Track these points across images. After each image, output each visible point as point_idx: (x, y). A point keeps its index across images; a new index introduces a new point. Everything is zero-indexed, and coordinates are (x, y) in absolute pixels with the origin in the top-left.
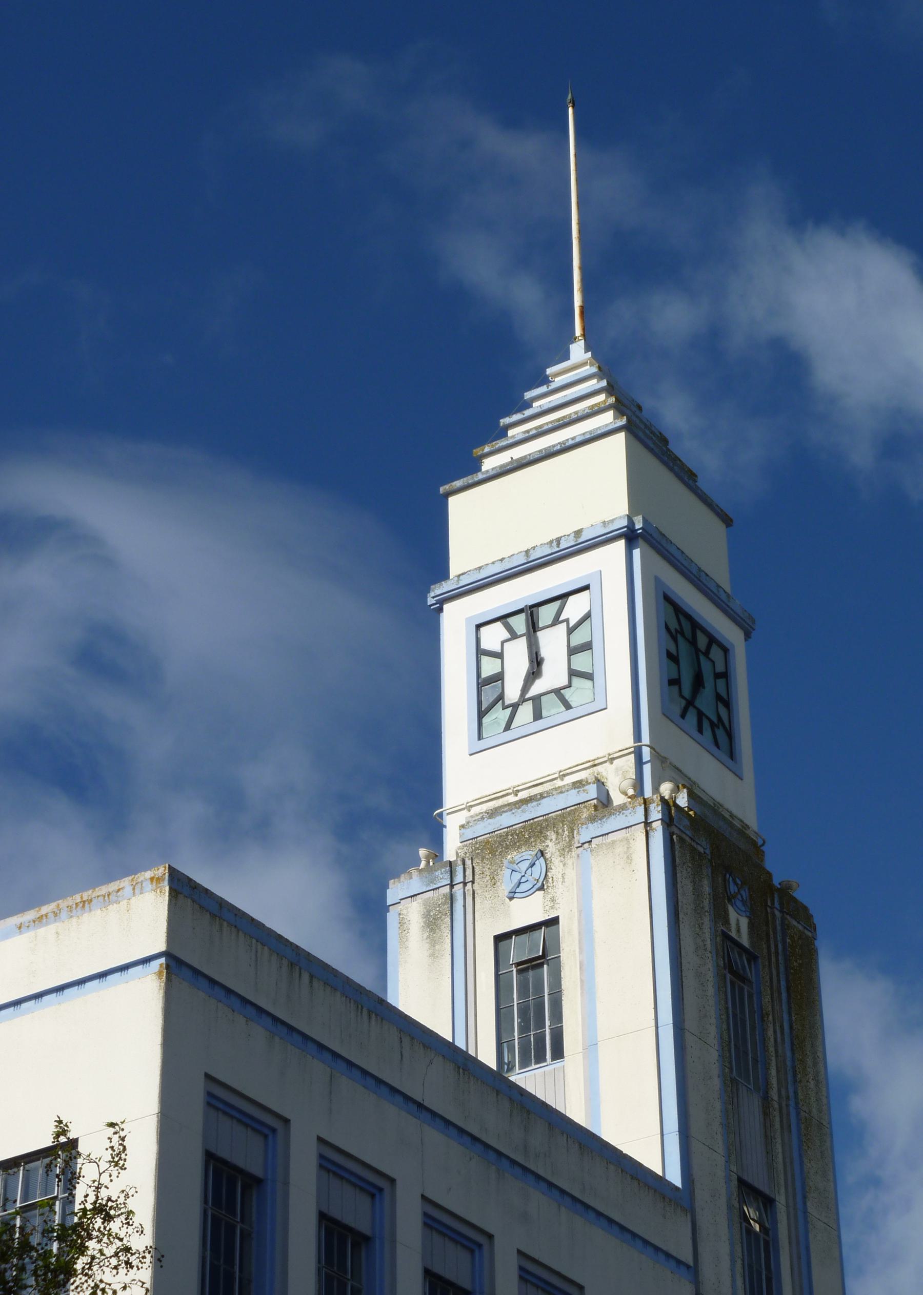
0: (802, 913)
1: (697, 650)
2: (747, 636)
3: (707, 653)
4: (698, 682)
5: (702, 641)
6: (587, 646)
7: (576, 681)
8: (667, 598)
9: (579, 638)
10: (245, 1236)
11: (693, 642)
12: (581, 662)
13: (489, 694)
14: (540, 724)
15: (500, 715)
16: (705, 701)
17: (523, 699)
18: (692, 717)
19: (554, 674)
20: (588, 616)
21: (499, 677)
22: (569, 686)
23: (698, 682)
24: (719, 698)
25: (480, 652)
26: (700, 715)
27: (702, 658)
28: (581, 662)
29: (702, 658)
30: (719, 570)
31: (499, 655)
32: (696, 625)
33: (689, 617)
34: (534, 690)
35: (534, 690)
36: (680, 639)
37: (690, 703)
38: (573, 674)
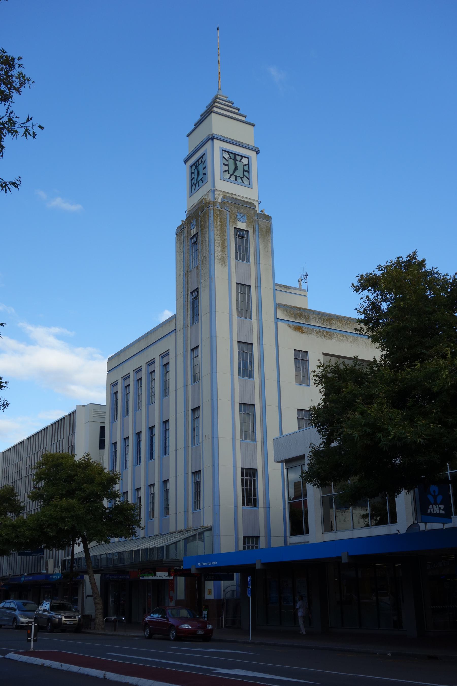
2: (258, 153)
4: (236, 169)
8: (223, 150)
14: (204, 183)
16: (239, 173)
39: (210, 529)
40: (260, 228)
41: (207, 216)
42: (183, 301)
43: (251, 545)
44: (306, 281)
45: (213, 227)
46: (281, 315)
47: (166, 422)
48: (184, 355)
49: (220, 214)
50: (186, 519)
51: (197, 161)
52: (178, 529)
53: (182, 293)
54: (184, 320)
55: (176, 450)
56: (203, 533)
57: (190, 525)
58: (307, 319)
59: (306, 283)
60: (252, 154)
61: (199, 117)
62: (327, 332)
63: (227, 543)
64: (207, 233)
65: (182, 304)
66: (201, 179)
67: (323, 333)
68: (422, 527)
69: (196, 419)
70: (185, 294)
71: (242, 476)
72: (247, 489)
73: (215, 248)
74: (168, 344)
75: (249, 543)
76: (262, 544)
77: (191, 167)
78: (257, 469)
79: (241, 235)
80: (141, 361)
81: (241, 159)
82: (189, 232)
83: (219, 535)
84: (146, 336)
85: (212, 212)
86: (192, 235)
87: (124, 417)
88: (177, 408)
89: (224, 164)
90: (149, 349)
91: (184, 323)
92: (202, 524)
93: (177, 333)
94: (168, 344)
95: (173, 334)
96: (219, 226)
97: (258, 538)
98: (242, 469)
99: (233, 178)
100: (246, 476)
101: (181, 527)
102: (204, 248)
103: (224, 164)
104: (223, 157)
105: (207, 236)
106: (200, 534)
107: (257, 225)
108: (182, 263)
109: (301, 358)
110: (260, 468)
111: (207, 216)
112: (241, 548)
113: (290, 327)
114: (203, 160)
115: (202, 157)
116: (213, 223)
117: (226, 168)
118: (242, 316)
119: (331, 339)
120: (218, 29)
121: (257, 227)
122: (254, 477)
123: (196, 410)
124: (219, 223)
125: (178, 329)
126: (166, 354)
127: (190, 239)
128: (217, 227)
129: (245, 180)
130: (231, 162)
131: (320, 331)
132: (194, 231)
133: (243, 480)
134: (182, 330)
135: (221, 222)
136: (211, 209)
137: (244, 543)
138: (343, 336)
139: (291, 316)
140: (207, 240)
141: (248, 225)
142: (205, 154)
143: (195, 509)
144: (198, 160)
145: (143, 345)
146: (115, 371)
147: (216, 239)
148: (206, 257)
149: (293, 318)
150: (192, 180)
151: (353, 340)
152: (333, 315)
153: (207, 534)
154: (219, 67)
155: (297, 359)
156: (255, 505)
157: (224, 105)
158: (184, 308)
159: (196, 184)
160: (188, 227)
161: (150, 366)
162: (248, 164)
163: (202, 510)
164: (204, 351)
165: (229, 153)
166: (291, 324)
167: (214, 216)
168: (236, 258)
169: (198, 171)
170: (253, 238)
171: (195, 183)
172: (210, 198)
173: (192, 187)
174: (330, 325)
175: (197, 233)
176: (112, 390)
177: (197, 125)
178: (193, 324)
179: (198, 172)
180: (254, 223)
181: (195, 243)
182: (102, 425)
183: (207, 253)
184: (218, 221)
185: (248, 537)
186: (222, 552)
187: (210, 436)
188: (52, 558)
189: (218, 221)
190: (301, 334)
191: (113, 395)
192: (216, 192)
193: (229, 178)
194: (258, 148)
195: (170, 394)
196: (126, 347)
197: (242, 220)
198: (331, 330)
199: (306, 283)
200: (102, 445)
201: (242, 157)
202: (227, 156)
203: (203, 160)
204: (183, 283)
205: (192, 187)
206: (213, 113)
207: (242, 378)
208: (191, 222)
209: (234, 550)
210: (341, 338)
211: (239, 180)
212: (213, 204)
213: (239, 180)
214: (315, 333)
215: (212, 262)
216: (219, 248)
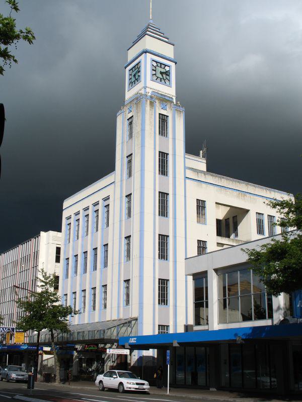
2: (176, 63)
39: (136, 319)
47: (106, 245)
51: (133, 68)
52: (113, 319)
56: (130, 322)
60: (173, 65)
63: (148, 329)
69: (130, 162)
71: (159, 284)
72: (162, 293)
75: (162, 330)
76: (171, 331)
78: (169, 280)
81: (165, 67)
83: (142, 323)
89: (153, 70)
92: (130, 316)
95: (113, 185)
97: (168, 326)
98: (159, 279)
100: (162, 284)
101: (115, 317)
103: (153, 70)
104: (153, 65)
106: (130, 322)
109: (201, 206)
110: (170, 152)
112: (157, 333)
114: (139, 67)
115: (137, 64)
117: (154, 72)
118: (162, 174)
122: (167, 285)
123: (129, 196)
125: (116, 181)
126: (107, 198)
129: (167, 81)
133: (159, 287)
137: (159, 330)
144: (135, 67)
153: (133, 322)
155: (198, 207)
157: (156, 34)
163: (131, 306)
164: (135, 241)
165: (156, 62)
168: (159, 215)
172: (143, 92)
182: (58, 246)
185: (162, 326)
192: (147, 88)
200: (58, 260)
201: (166, 66)
202: (155, 64)
203: (139, 67)
206: (146, 36)
207: (161, 176)
209: (152, 334)
211: (163, 81)
213: (163, 81)
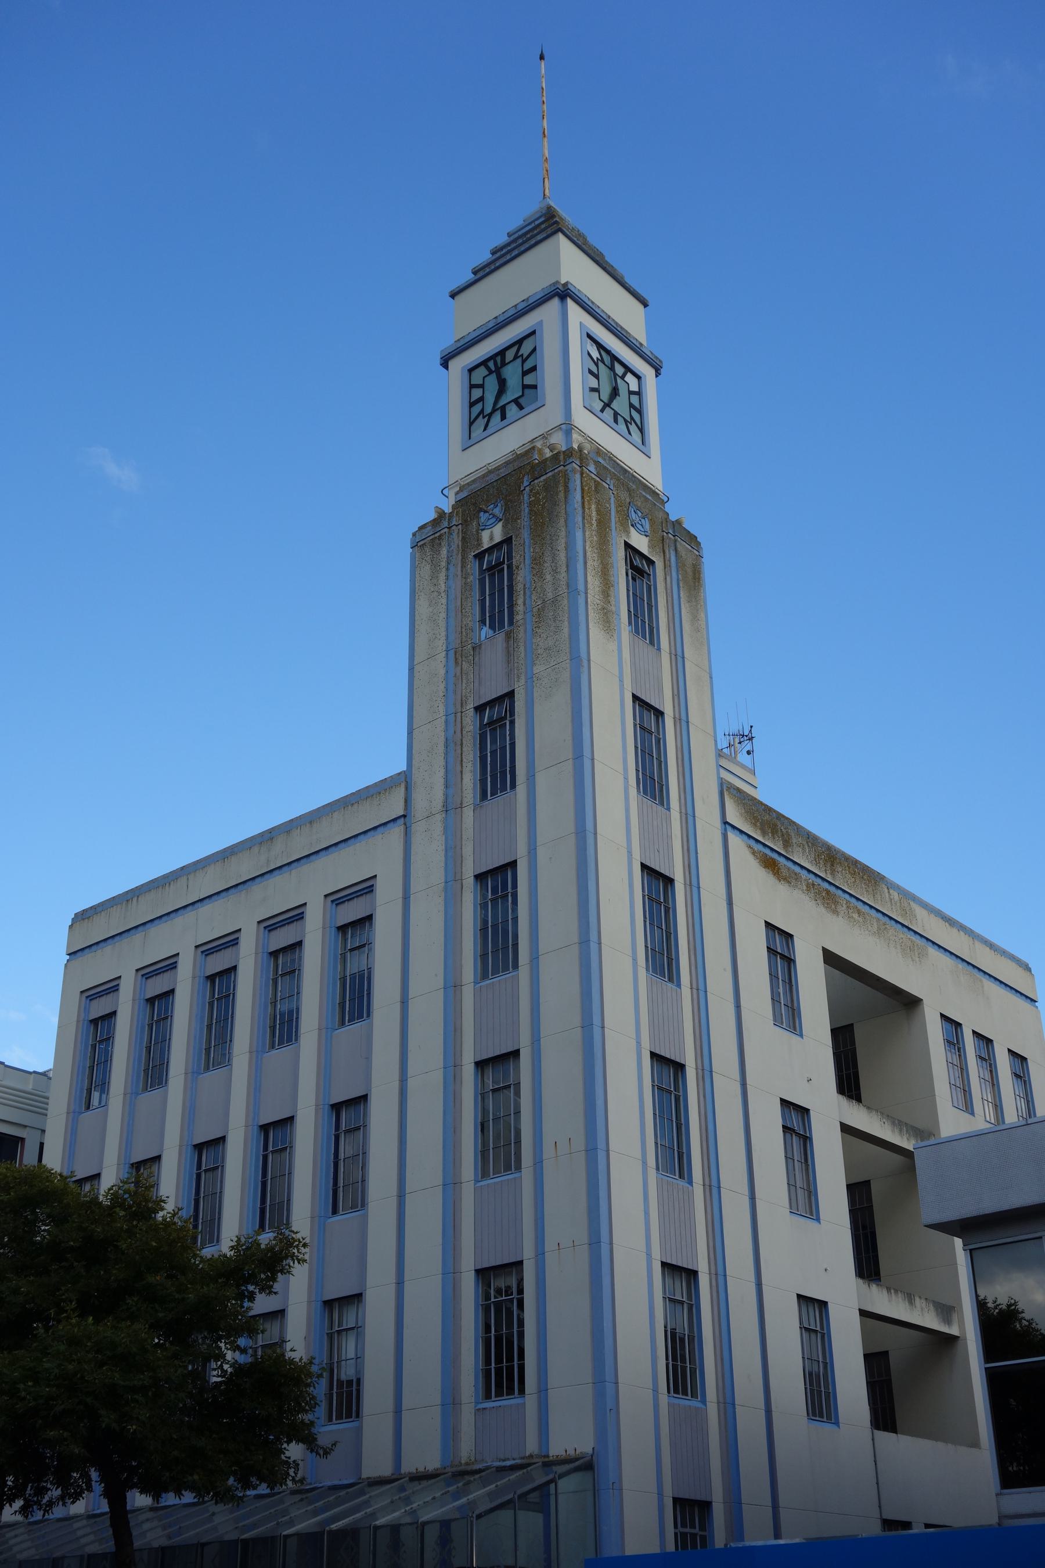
0: (692, 539)
1: (615, 375)
2: (658, 373)
3: (623, 377)
4: (615, 392)
5: (619, 370)
6: (534, 369)
7: (527, 391)
8: (589, 336)
9: (528, 365)
10: (693, 1372)
11: (612, 368)
12: (529, 380)
13: (477, 409)
14: (505, 422)
15: (481, 422)
16: (620, 405)
17: (494, 411)
18: (608, 414)
19: (513, 391)
20: (534, 350)
21: (481, 399)
22: (523, 395)
23: (615, 392)
24: (631, 406)
25: (472, 387)
26: (616, 415)
27: (619, 380)
28: (529, 380)
29: (619, 380)
30: (638, 331)
31: (482, 386)
32: (614, 358)
33: (608, 352)
34: (501, 403)
35: (501, 403)
36: (600, 364)
37: (607, 405)
38: (525, 387)
39: (585, 1465)
40: (681, 565)
41: (561, 488)
42: (446, 730)
43: (688, 1530)
44: (749, 748)
45: (580, 519)
46: (734, 816)
48: (446, 890)
49: (597, 491)
50: (450, 1433)
53: (442, 709)
54: (446, 787)
55: (401, 1197)
57: (466, 1450)
58: (787, 844)
59: (749, 753)
61: (486, 256)
62: (828, 892)
64: (563, 534)
65: (443, 739)
66: (516, 401)
67: (820, 893)
68: (733, 1545)
70: (452, 710)
73: (589, 579)
74: (379, 858)
77: (471, 371)
79: (639, 567)
80: (211, 923)
82: (468, 540)
83: (618, 1487)
84: (267, 838)
85: (576, 481)
86: (486, 546)
87: (137, 1094)
88: (411, 1061)
89: (591, 372)
90: (276, 879)
91: (446, 796)
93: (414, 828)
94: (379, 858)
95: (397, 830)
96: (594, 522)
97: (705, 1506)
99: (608, 414)
102: (548, 577)
105: (562, 542)
107: (673, 553)
108: (442, 624)
111: (561, 488)
113: (754, 853)
116: (580, 509)
119: (835, 912)
120: (542, 58)
121: (673, 558)
124: (594, 514)
127: (475, 556)
128: (592, 525)
130: (603, 371)
131: (813, 885)
132: (493, 534)
134: (439, 817)
135: (598, 511)
136: (574, 471)
138: (859, 912)
139: (755, 825)
140: (562, 556)
141: (651, 546)
142: (534, 333)
143: (488, 1396)
145: (244, 868)
146: (88, 956)
147: (589, 554)
148: (555, 600)
149: (759, 832)
150: (472, 405)
151: (879, 929)
152: (838, 851)
154: (546, 144)
156: (694, 1395)
158: (446, 754)
159: (490, 415)
160: (465, 523)
161: (150, 981)
162: (638, 394)
163: (530, 1401)
166: (758, 847)
167: (583, 490)
169: (502, 380)
170: (663, 584)
171: (488, 410)
173: (471, 423)
174: (832, 874)
175: (508, 541)
176: (87, 1010)
177: (482, 273)
178: (484, 796)
179: (502, 383)
180: (666, 546)
181: (495, 570)
183: (563, 589)
184: (593, 507)
186: (629, 1552)
187: (579, 1143)
188: (366, 1504)
189: (593, 507)
190: (777, 882)
191: (93, 1029)
193: (602, 411)
194: (661, 361)
195: (235, 1061)
196: (165, 877)
197: (640, 527)
198: (840, 892)
199: (749, 753)
204: (446, 679)
205: (471, 423)
208: (481, 510)
209: (658, 1551)
210: (856, 916)
212: (581, 460)
213: (622, 426)
214: (805, 888)
215: (582, 618)
216: (597, 583)
